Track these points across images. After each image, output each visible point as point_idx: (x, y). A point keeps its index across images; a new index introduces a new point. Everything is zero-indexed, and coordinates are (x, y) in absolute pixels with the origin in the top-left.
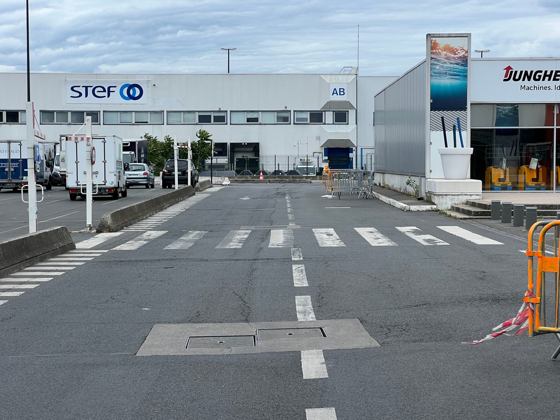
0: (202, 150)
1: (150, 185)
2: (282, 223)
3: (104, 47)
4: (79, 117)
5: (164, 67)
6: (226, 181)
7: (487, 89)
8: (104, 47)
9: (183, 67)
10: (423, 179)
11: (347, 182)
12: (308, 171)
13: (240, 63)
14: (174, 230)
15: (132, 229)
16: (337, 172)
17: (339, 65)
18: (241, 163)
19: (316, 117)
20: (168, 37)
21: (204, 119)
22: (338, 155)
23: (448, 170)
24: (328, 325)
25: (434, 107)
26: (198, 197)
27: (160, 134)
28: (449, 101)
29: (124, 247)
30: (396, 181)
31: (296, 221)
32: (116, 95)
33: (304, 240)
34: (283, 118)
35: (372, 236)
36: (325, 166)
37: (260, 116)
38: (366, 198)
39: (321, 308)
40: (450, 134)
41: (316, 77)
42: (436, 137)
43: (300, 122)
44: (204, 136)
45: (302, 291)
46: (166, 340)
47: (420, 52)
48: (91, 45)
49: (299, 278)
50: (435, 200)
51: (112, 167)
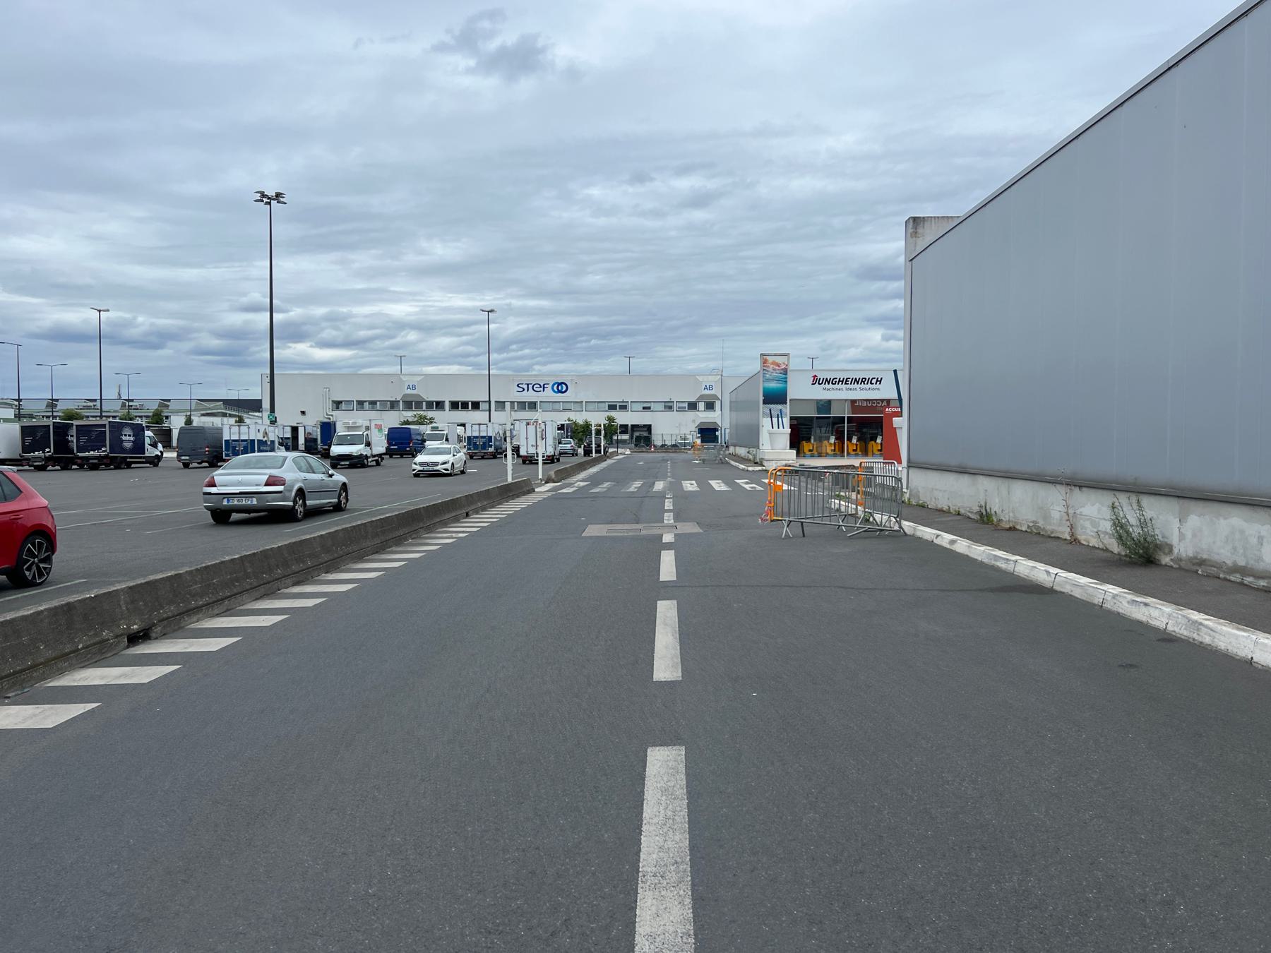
0: (611, 430)
1: (575, 454)
2: (664, 478)
3: (536, 352)
4: (523, 406)
5: (583, 368)
6: (628, 452)
7: (801, 390)
8: (536, 352)
9: (596, 367)
10: (172, 406)
11: (711, 451)
12: (685, 445)
13: (639, 364)
14: (595, 481)
15: (567, 481)
16: (706, 445)
17: (712, 365)
18: (638, 438)
19: (693, 406)
20: (584, 345)
21: (612, 407)
22: (708, 433)
23: (775, 445)
24: (679, 525)
25: (764, 403)
26: (609, 462)
27: (580, 418)
28: (775, 398)
29: (564, 491)
30: (742, 451)
31: (672, 477)
32: (549, 390)
33: (676, 487)
34: (669, 407)
35: (717, 485)
36: (699, 441)
37: (652, 405)
38: (723, 462)
39: (676, 519)
40: (775, 420)
41: (691, 377)
42: (766, 422)
43: (681, 409)
44: (611, 419)
45: (669, 511)
46: (593, 530)
47: (757, 366)
48: (527, 351)
49: (668, 505)
50: (765, 463)
51: (550, 441)
